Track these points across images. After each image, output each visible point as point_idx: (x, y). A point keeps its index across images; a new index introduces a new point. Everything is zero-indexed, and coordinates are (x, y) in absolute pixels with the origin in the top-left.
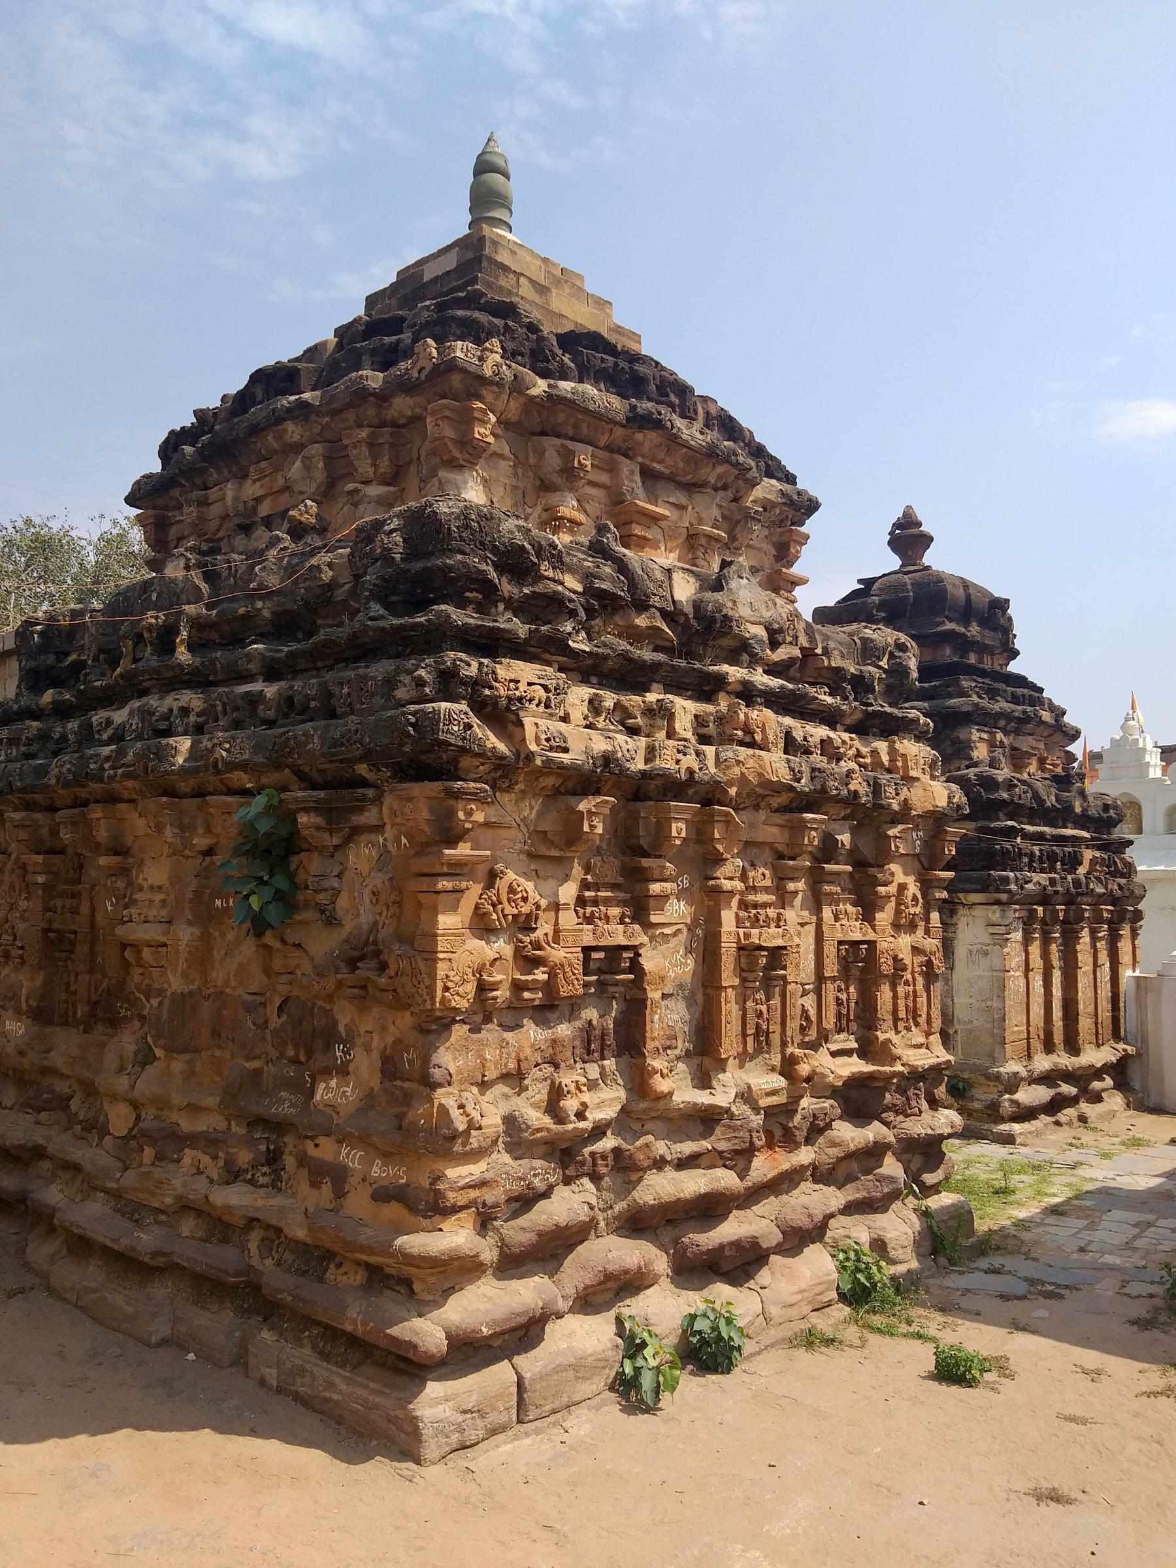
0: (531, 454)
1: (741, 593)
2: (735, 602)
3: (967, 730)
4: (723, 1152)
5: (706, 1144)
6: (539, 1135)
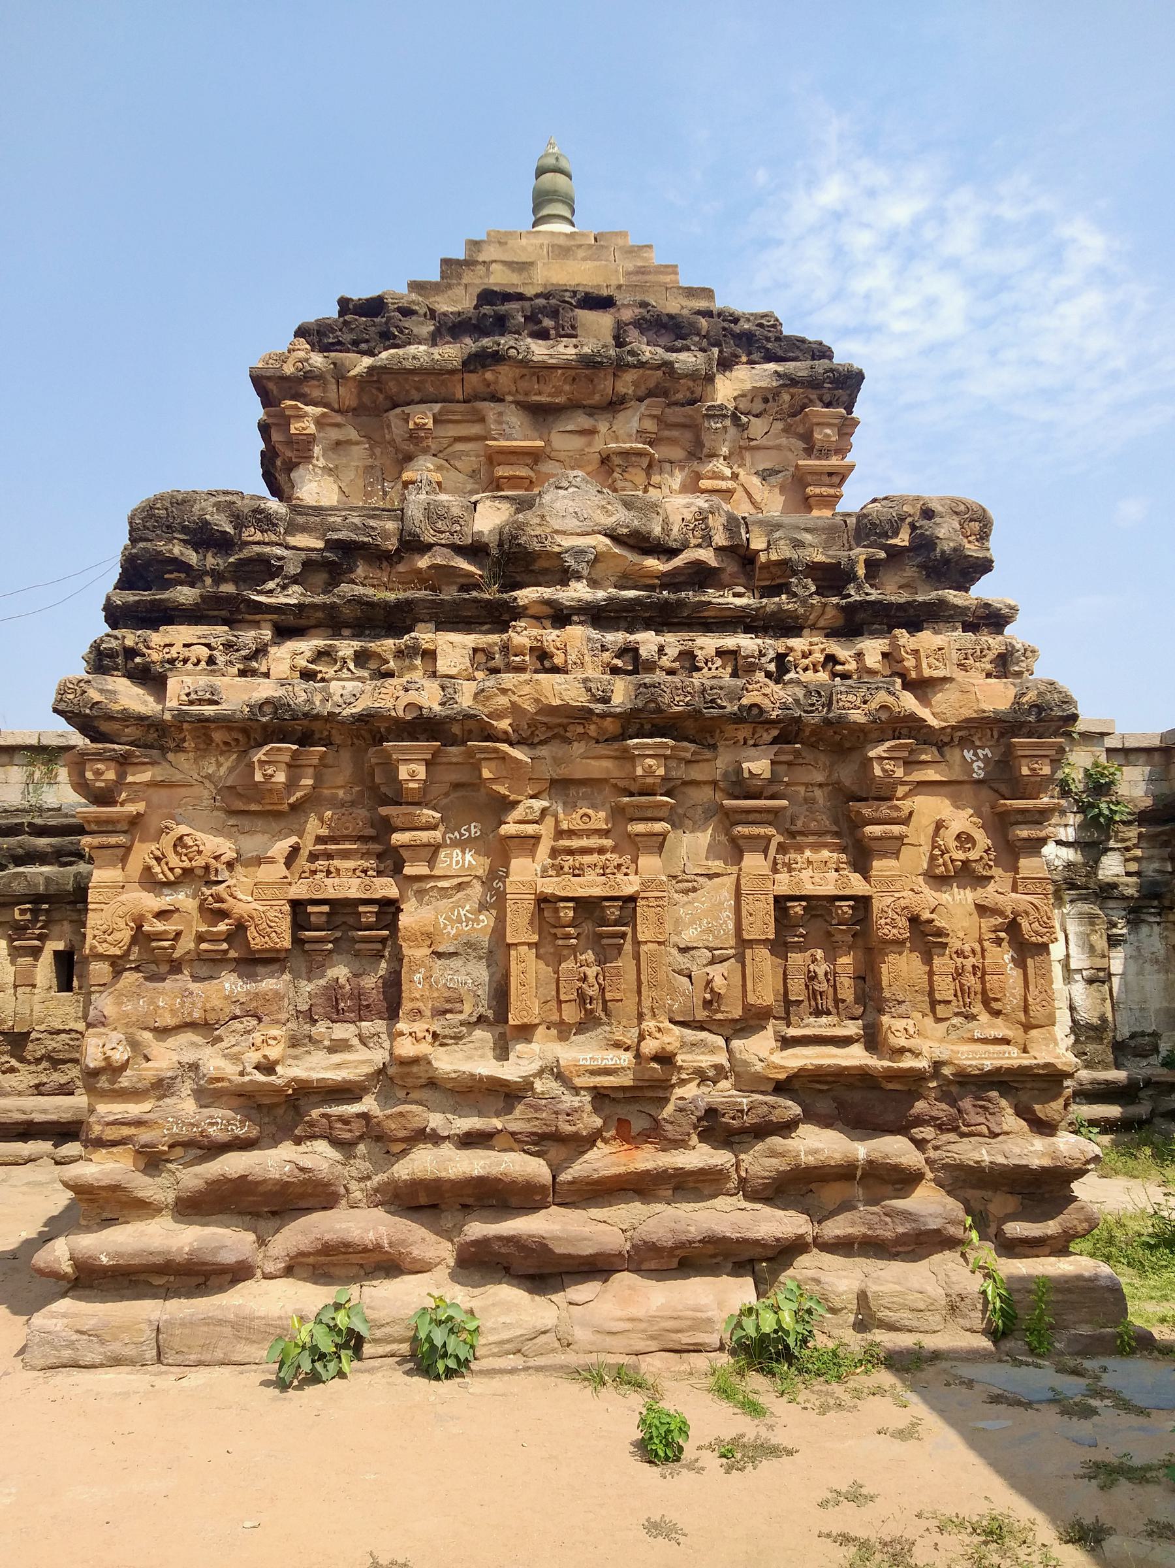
1: (557, 505)
2: (542, 517)
4: (517, 1134)
5: (497, 1123)
6: (220, 1085)
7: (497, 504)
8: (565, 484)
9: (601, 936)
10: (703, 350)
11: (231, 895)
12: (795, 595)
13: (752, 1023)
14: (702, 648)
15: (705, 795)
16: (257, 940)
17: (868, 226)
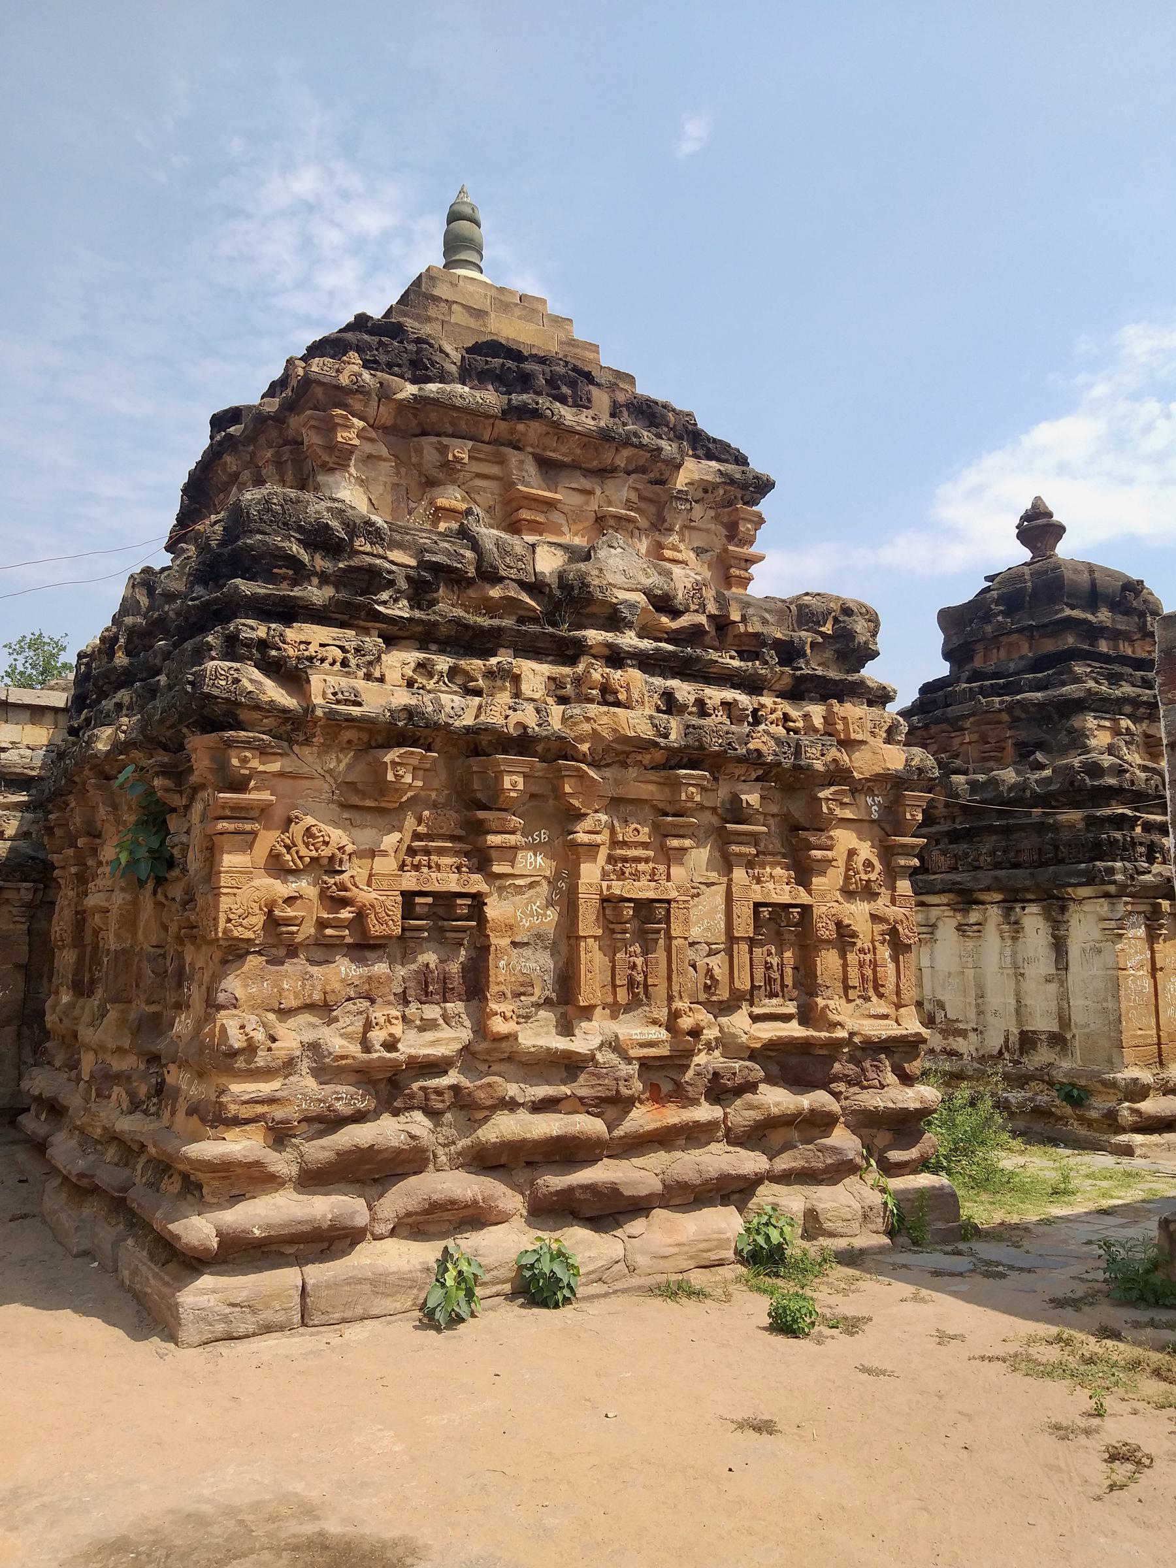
0: (413, 454)
1: (611, 561)
2: (601, 570)
3: (1081, 717)
5: (566, 1090)
6: (344, 1062)
8: (616, 545)
9: (647, 932)
11: (355, 885)
16: (377, 928)
17: (338, 225)
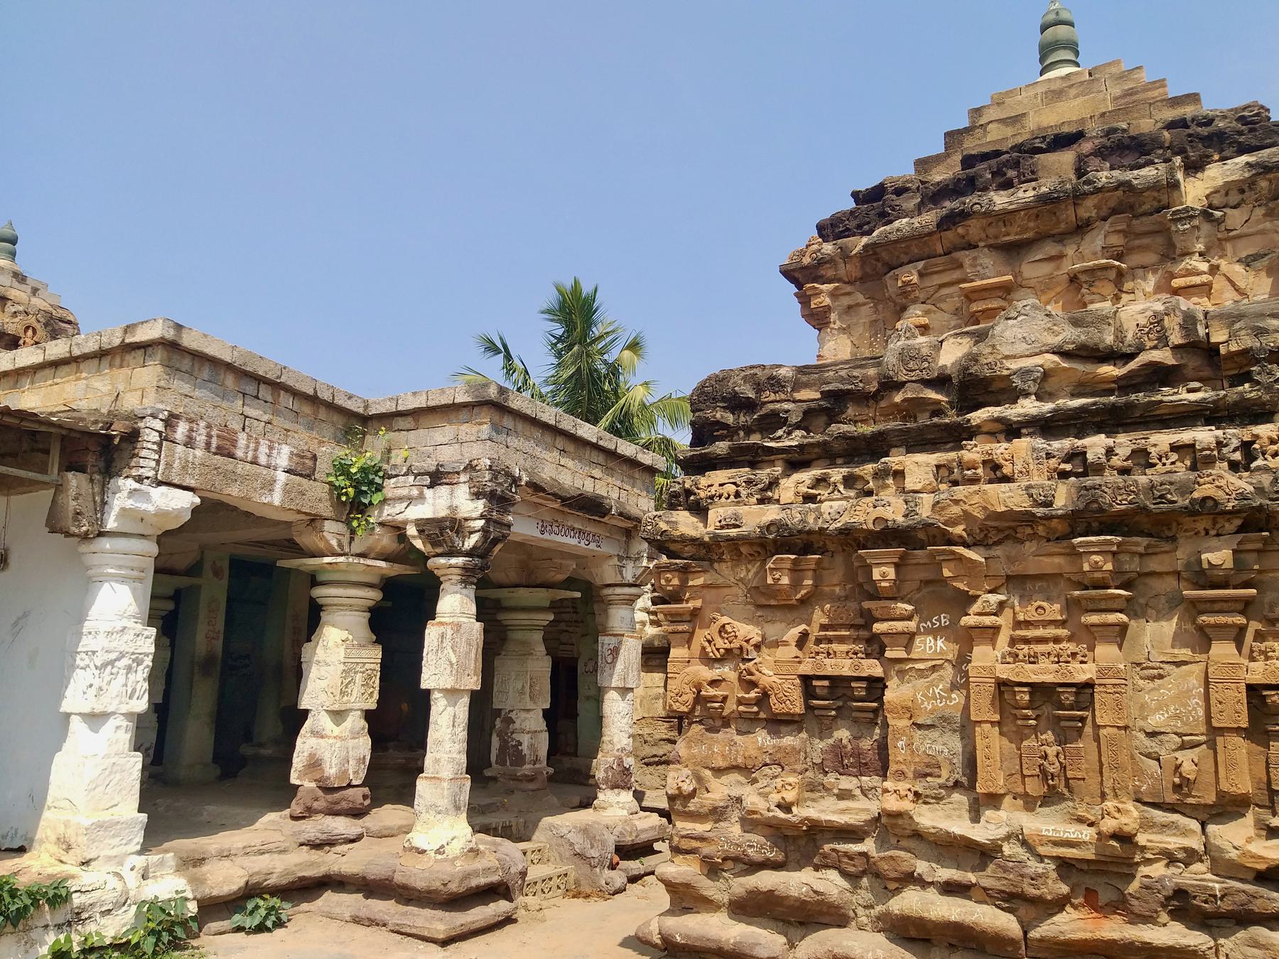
1: (1007, 334)
2: (993, 346)
5: (972, 877)
7: (959, 340)
8: (1014, 314)
9: (1059, 718)
10: (1167, 161)
12: (1258, 383)
13: (1229, 809)
14: (1155, 445)
15: (1169, 584)
